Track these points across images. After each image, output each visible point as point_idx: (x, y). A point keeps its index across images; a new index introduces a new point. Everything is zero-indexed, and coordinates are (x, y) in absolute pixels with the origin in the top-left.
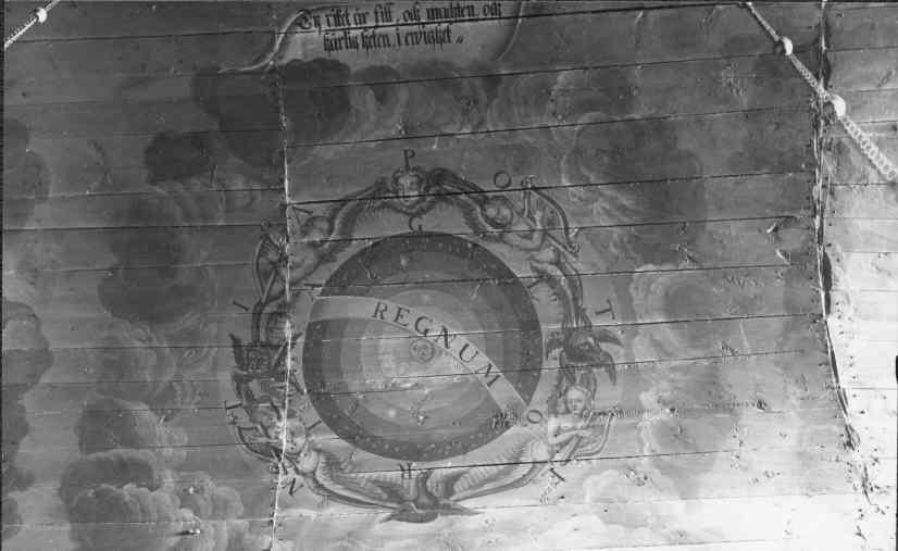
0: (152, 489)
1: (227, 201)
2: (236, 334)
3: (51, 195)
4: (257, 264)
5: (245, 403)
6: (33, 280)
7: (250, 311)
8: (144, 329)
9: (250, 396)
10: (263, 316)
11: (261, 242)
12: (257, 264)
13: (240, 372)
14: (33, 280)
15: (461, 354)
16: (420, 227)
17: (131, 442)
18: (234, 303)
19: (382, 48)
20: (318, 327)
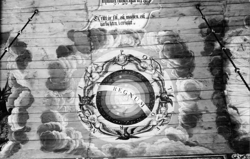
4: (85, 77)
5: (82, 111)
7: (83, 89)
9: (83, 109)
11: (85, 72)
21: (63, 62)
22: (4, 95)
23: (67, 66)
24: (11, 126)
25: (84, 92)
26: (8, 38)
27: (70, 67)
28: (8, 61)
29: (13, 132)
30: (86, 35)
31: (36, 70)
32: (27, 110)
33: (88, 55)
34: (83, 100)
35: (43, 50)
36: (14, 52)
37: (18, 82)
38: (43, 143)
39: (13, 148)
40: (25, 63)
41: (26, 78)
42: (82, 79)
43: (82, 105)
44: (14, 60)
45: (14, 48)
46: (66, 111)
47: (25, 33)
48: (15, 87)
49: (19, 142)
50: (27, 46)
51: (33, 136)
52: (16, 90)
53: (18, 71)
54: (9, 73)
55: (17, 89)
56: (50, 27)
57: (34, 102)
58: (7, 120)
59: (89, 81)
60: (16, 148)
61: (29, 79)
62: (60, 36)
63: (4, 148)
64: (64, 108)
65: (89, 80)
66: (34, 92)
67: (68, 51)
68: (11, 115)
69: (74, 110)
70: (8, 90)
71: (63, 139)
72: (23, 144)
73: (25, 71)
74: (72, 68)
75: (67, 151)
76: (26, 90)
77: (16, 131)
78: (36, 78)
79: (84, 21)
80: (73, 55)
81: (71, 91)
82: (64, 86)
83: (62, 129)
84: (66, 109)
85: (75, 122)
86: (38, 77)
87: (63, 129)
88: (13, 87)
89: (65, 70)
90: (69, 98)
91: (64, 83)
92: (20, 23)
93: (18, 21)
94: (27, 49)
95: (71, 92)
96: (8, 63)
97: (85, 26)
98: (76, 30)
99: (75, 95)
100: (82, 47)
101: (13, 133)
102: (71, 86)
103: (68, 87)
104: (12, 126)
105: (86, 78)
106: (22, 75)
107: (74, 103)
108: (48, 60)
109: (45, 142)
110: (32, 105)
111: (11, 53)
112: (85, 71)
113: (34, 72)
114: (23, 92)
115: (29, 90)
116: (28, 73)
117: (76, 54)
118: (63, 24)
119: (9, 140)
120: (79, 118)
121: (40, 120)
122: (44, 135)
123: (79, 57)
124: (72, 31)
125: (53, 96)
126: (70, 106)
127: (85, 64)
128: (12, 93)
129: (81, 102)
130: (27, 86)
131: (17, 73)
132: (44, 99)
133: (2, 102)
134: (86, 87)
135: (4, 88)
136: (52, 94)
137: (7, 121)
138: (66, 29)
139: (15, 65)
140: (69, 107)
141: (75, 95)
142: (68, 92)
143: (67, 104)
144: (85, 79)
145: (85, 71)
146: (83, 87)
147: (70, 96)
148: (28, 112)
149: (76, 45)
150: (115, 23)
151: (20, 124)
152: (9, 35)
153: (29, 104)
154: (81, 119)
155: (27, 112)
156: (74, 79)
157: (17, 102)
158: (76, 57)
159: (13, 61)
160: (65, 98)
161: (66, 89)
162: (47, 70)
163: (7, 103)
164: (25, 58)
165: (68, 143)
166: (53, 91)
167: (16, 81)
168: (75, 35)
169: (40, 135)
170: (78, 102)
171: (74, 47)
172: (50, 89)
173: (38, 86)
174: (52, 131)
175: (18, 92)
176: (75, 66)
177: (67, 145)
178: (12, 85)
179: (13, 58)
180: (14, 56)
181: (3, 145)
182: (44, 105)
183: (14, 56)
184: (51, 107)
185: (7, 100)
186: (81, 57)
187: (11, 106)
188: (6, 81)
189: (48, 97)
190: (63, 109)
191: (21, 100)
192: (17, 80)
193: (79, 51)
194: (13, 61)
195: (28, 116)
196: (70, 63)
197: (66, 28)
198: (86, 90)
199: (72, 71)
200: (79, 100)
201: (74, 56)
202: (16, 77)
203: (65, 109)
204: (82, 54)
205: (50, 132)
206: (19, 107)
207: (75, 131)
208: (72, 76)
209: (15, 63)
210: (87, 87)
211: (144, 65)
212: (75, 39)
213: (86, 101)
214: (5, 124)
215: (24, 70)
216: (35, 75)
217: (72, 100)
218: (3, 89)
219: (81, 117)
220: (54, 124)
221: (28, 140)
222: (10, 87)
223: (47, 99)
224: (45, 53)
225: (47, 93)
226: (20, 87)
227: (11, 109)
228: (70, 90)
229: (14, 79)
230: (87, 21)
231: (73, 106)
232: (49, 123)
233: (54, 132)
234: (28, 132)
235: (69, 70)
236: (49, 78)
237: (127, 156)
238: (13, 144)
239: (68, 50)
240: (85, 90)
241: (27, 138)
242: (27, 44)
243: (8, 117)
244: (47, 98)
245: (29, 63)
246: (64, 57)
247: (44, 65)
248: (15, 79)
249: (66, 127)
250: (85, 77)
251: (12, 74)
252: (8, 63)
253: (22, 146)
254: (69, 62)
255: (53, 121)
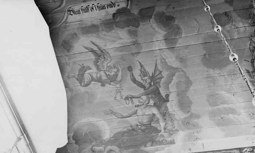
0: (239, 115)
1: (238, 31)
3: (183, 36)
4: (250, 48)
6: (181, 61)
7: (250, 61)
8: (218, 71)
12: (250, 48)
13: (252, 80)
14: (181, 61)
15: (126, 104)
16: (103, 76)
17: (224, 103)
18: (244, 60)
22: (155, 81)
64: (232, 87)
70: (158, 74)
128: (163, 77)
137: (167, 109)
150: (102, 8)
211: (250, 150)
214: (166, 113)
220: (228, 107)
227: (167, 96)
233: (231, 116)
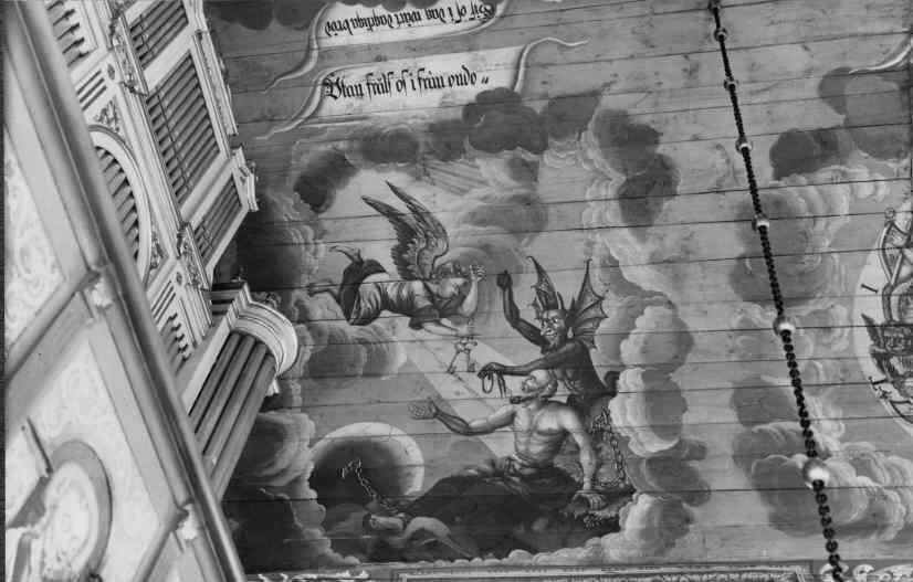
2: (867, 314)
5: (891, 379)
7: (880, 292)
9: (892, 371)
10: (893, 298)
11: (886, 229)
19: (349, 19)
20: (254, 164)
21: (796, 194)
22: (580, 325)
23: (811, 209)
24: (627, 440)
25: (887, 307)
26: (593, 112)
27: (821, 211)
28: (588, 197)
29: (641, 459)
30: (894, 86)
31: (692, 228)
32: (675, 377)
33: (898, 162)
34: (887, 339)
35: (719, 152)
36: (613, 164)
37: (628, 274)
38: (771, 503)
39: (664, 516)
40: (652, 202)
41: (655, 261)
42: (875, 258)
43: (887, 356)
44: (611, 193)
45: (611, 149)
46: (823, 380)
47: (659, 92)
48: (616, 293)
49: (680, 498)
50: (662, 138)
51: (723, 475)
52: (619, 304)
53: (626, 232)
54: (590, 244)
55: (626, 300)
56: (753, 65)
57: (694, 348)
58: (608, 415)
59: (902, 262)
60: (671, 522)
61: (668, 261)
62: (789, 94)
63: (629, 519)
64: (815, 367)
65: (904, 257)
66: (691, 309)
67: (818, 149)
68: (619, 395)
69: (855, 377)
71: (842, 484)
72: (699, 504)
73: (650, 234)
74: (830, 215)
75: (880, 533)
76: (658, 303)
77: (650, 456)
78: (691, 257)
79: (892, 33)
80: (837, 167)
81: (832, 303)
82: (802, 283)
83: (828, 446)
84: (821, 372)
85: (872, 421)
86: (704, 252)
87: (831, 449)
88: (611, 295)
89: (802, 224)
90: (828, 329)
91: (802, 274)
92: (642, 56)
93: (637, 47)
94: (660, 150)
95: (832, 306)
96: (589, 206)
97: (894, 49)
98: (855, 65)
99: (849, 318)
100: (875, 132)
101: (644, 464)
102: (830, 286)
103: (818, 288)
104: (633, 439)
105: (888, 253)
106: (639, 248)
107: (851, 348)
108: (735, 187)
109: (776, 499)
110: (687, 362)
111: (602, 169)
112: (886, 225)
113: (685, 235)
114: (648, 310)
115: (670, 304)
116: (661, 239)
117: (849, 163)
118: (806, 48)
119: (634, 491)
120: (889, 409)
121: (731, 416)
122: (762, 470)
123: (857, 170)
124: (842, 73)
125: (760, 323)
126: (839, 359)
127: (886, 198)
128: (607, 317)
129: (879, 345)
130: (659, 290)
131: (624, 242)
132: (731, 337)
133: (574, 349)
134: (889, 289)
135: (576, 299)
136: (759, 316)
137: (610, 420)
138: (818, 70)
139: (612, 213)
140: (834, 364)
141: (849, 318)
142: (819, 307)
143: (821, 352)
144: (884, 255)
145: (886, 225)
146: (880, 285)
147: (830, 324)
148: (680, 384)
149: (849, 126)
151: (662, 430)
152: (597, 103)
153: (676, 357)
154: (896, 409)
155: (675, 384)
156: (841, 260)
157: (630, 349)
158: (847, 170)
159: (606, 200)
160: (812, 333)
161: (812, 298)
162: (733, 225)
163: (592, 352)
164: (649, 188)
165: (871, 501)
166: (763, 306)
167: (621, 272)
168: (850, 88)
169: (748, 470)
170: (863, 343)
171: (843, 135)
172: (747, 299)
173: (702, 288)
174: (790, 456)
175: (630, 312)
176: (843, 206)
177: (869, 509)
178: (606, 285)
179: (607, 186)
180: (610, 179)
181: (619, 508)
182: (734, 358)
183: (610, 179)
184: (764, 365)
185: (593, 342)
186: (870, 173)
187: (612, 362)
188: (583, 272)
189: (744, 326)
190: (813, 371)
191: (646, 343)
192: (622, 269)
193: (861, 147)
194: (606, 200)
195: (684, 400)
196: (825, 197)
197: (816, 62)
198: (894, 300)
199: (830, 228)
200: (869, 338)
201: (843, 168)
202: (616, 258)
203: (818, 374)
204: (874, 161)
205: (783, 461)
206: (640, 366)
207: (882, 455)
208: (830, 246)
209: (615, 204)
210: (896, 285)
212: (850, 103)
213: (898, 340)
214: (602, 430)
215: (649, 230)
216: (689, 249)
217: (841, 336)
218: (573, 301)
219: (892, 402)
220: (791, 430)
221: (710, 491)
222: (601, 295)
223: (742, 337)
224: (728, 161)
225: (740, 313)
226: (636, 294)
227: (613, 376)
228: (826, 299)
229: (611, 265)
230: (906, 32)
231: (846, 360)
232: (769, 427)
234: (698, 459)
235: (821, 224)
236: (741, 258)
237: (103, 476)
238: (655, 505)
239: (818, 146)
240: (887, 297)
241: (703, 482)
242: (662, 134)
243: (607, 405)
244: (743, 330)
245: (667, 204)
246: (799, 173)
247: (721, 207)
248: (615, 265)
249: (842, 440)
250: (884, 249)
251: (604, 244)
252: (589, 206)
253: (696, 511)
254: (821, 192)
255: (783, 419)
